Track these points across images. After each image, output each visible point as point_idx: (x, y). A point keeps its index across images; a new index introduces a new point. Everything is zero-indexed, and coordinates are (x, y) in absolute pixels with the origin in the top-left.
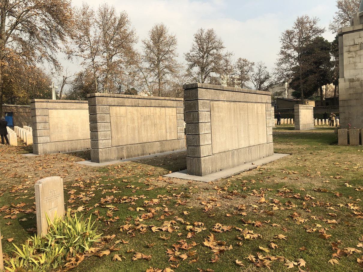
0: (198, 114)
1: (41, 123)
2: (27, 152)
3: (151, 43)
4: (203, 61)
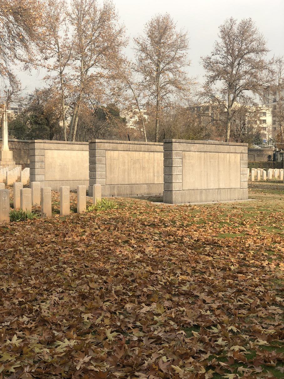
0: (172, 161)
3: (148, 42)
4: (232, 72)
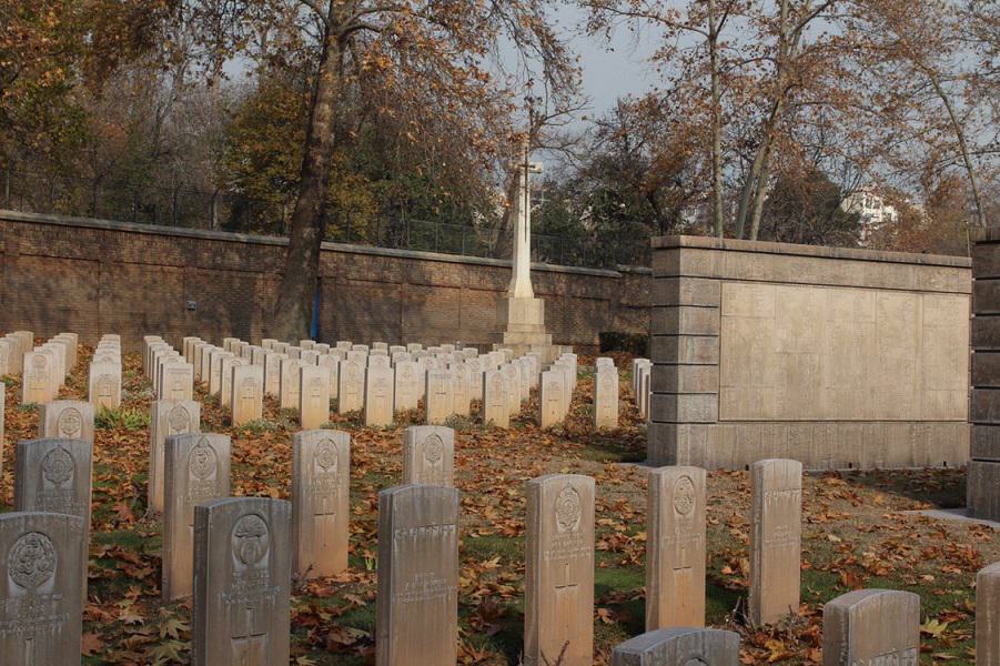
1: (695, 339)
2: (616, 457)
